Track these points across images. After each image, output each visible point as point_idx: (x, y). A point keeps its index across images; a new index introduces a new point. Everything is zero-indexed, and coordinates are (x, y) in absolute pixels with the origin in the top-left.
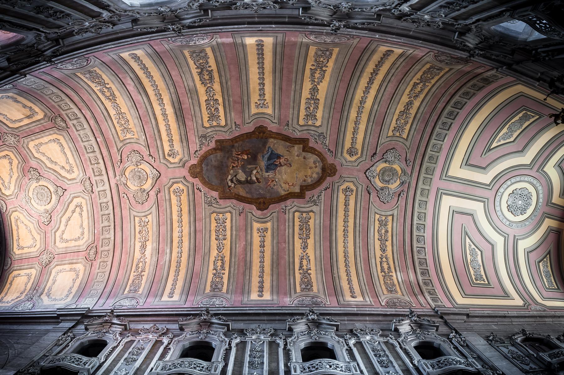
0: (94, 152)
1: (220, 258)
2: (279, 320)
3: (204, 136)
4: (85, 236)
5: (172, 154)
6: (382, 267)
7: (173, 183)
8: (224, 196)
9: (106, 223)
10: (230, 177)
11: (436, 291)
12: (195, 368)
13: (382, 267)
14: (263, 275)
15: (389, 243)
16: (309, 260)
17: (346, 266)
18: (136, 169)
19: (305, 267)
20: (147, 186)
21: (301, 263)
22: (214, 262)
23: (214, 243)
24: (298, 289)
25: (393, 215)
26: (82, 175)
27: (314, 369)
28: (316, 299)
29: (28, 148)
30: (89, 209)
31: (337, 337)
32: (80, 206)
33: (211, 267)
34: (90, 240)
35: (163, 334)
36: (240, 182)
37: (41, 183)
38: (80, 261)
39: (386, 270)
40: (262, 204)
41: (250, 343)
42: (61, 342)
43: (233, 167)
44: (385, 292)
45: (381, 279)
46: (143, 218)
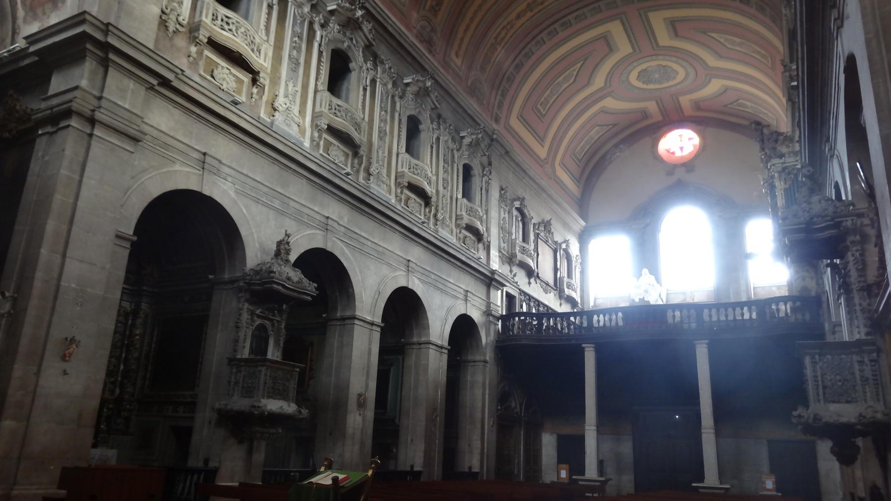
2: (402, 56)
15: (529, 14)
24: (427, 8)
27: (226, 27)
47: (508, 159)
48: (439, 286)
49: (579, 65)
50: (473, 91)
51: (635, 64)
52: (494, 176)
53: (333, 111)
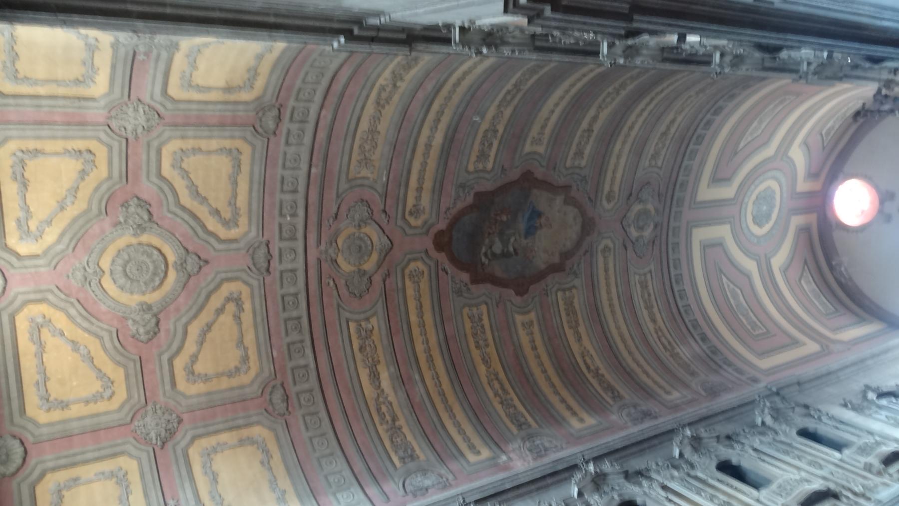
0: (295, 191)
1: (493, 377)
3: (462, 186)
4: (252, 364)
5: (416, 212)
6: (663, 344)
7: (409, 261)
8: (476, 280)
9: (294, 336)
10: (484, 250)
13: (663, 344)
15: (655, 310)
17: (630, 353)
18: (357, 235)
19: (592, 367)
20: (369, 265)
21: (586, 363)
23: (476, 354)
25: (650, 272)
26: (253, 233)
29: (159, 152)
30: (258, 307)
32: (237, 300)
33: (491, 394)
34: (266, 373)
36: (494, 255)
37: (145, 238)
38: (255, 419)
40: (522, 284)
43: (489, 234)
46: (363, 324)
49: (724, 279)
50: (713, 392)
51: (744, 226)
52: (824, 408)
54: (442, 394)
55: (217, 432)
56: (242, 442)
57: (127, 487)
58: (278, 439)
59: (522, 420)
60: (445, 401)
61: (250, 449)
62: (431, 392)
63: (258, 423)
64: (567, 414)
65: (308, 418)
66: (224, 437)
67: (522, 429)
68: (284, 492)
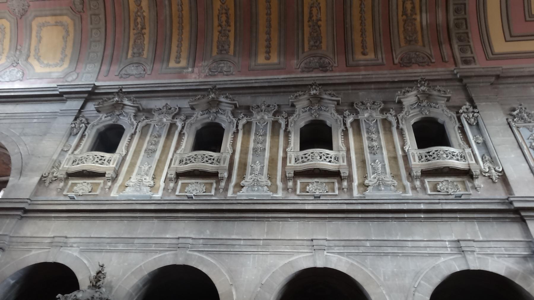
1: (224, 11)
2: (284, 92)
6: (404, 8)
11: (470, 35)
12: (207, 161)
13: (404, 8)
14: (270, 30)
16: (320, 8)
17: (362, 11)
19: (314, 18)
21: (311, 13)
22: (218, 16)
28: (323, 59)
31: (336, 114)
33: (216, 23)
35: (176, 114)
39: (409, 12)
41: (255, 124)
42: (75, 131)
44: (403, 44)
45: (401, 24)
47: (504, 81)
48: (380, 250)
53: (301, 160)
54: (181, 17)
55: (46, 16)
56: (57, 24)
57: (4, 35)
58: (75, 25)
59: (226, 47)
60: (181, 23)
61: (60, 28)
62: (173, 14)
63: (66, 15)
64: (262, 49)
65: (93, 17)
66: (49, 19)
67: (221, 53)
68: (66, 56)
